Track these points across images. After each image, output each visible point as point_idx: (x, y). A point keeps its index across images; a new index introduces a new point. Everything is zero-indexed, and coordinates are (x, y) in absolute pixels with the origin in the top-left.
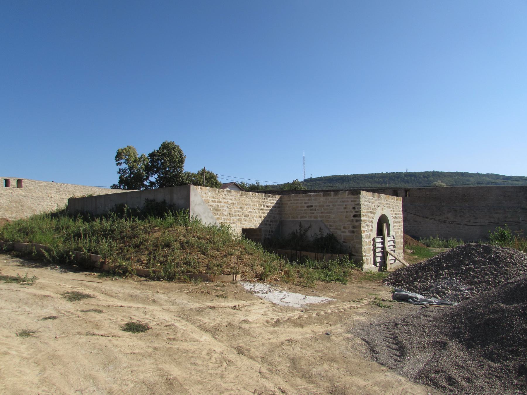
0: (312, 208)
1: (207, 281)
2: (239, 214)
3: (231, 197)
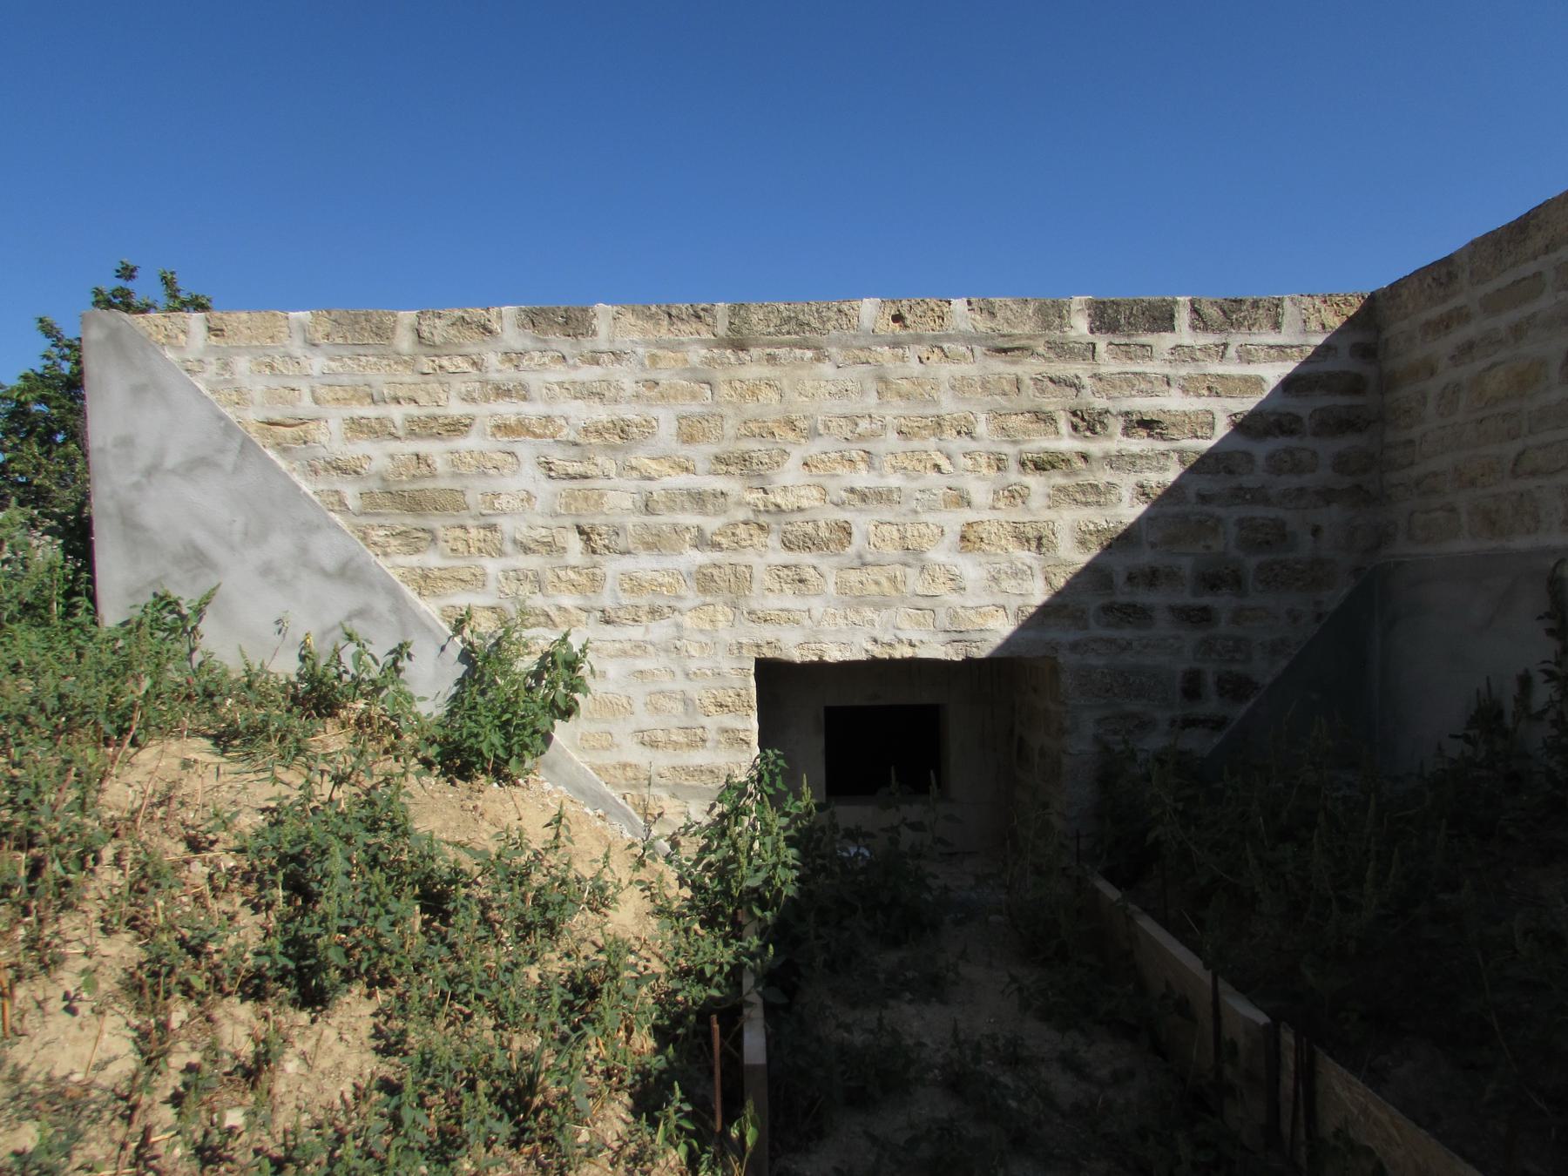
2: (711, 524)
3: (588, 373)
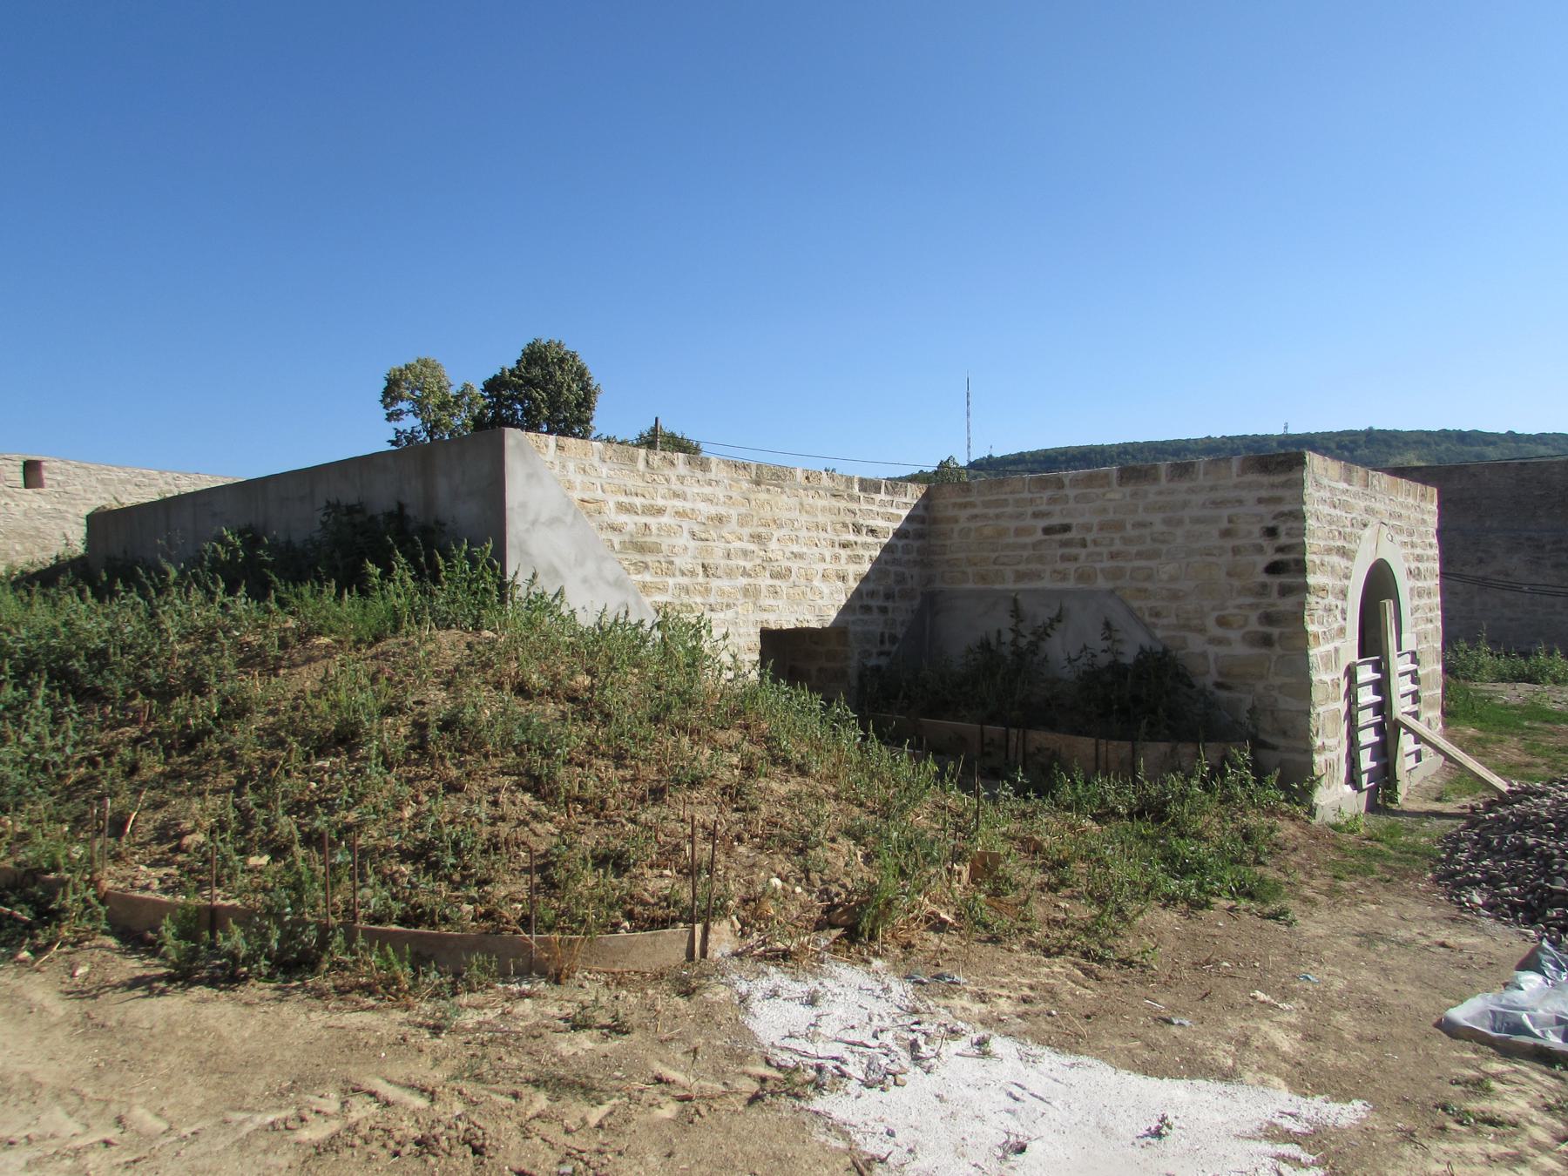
0: (1067, 536)
1: (524, 973)
2: (749, 565)
3: (707, 490)
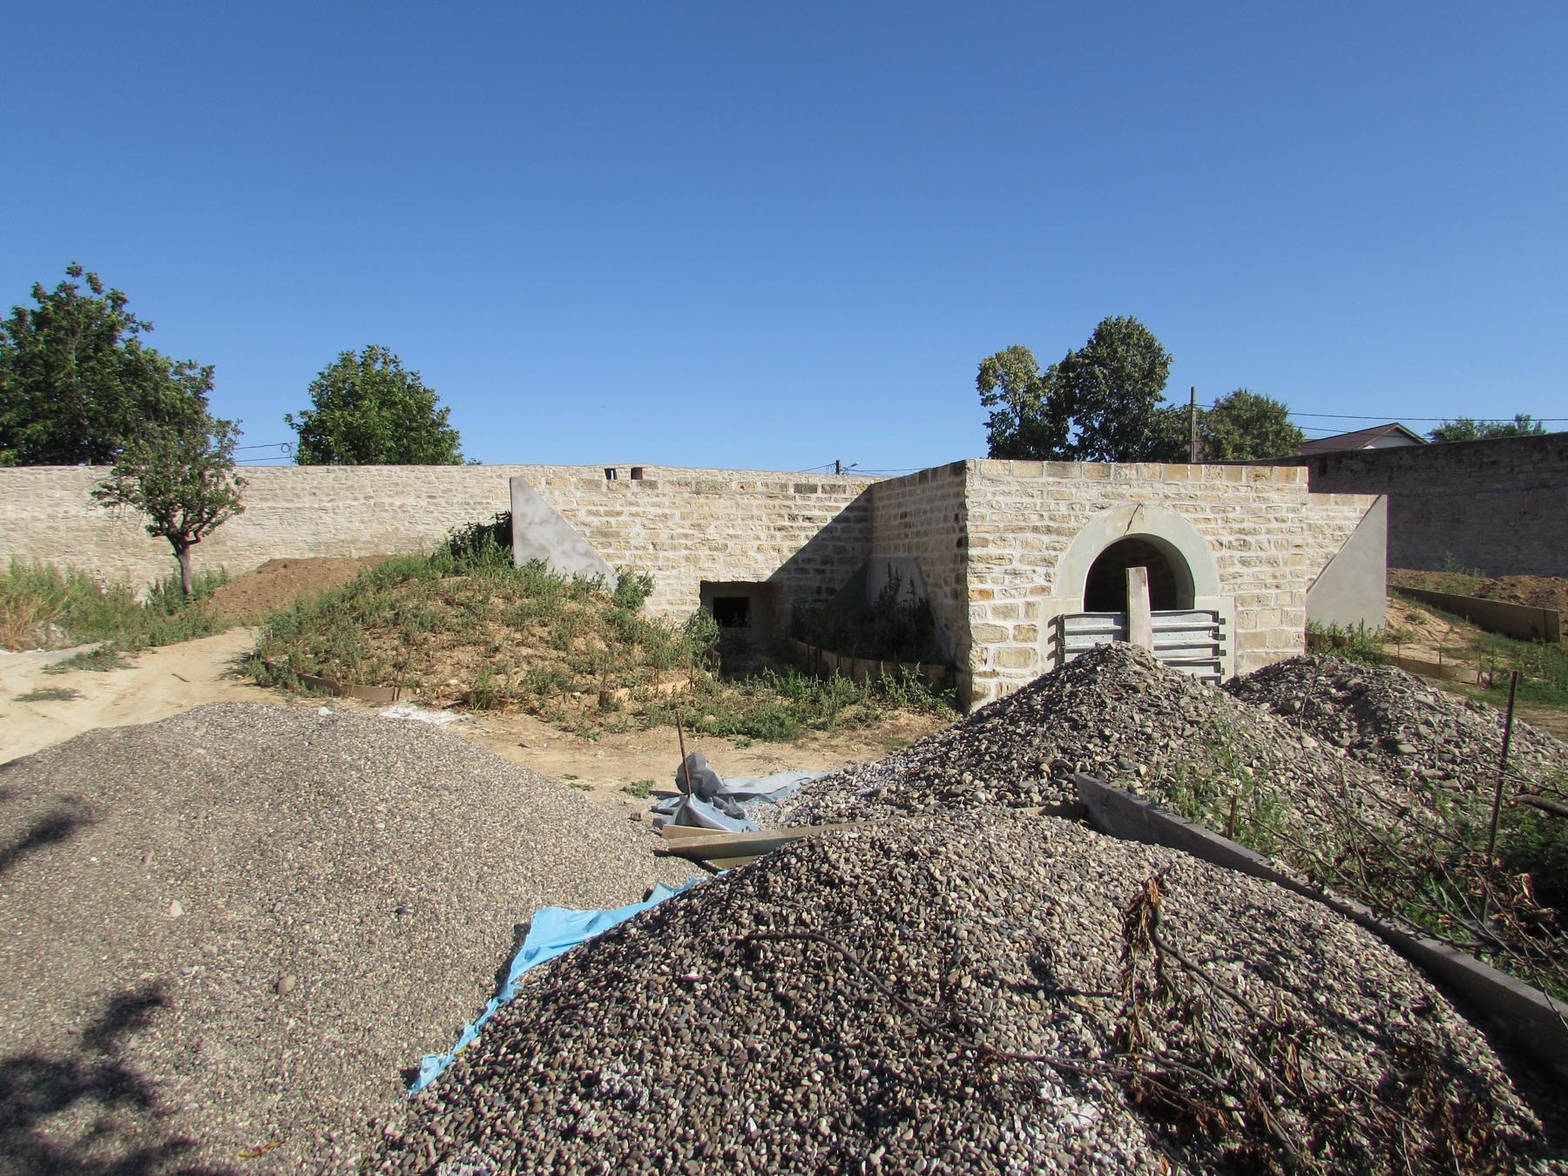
3: (656, 500)
